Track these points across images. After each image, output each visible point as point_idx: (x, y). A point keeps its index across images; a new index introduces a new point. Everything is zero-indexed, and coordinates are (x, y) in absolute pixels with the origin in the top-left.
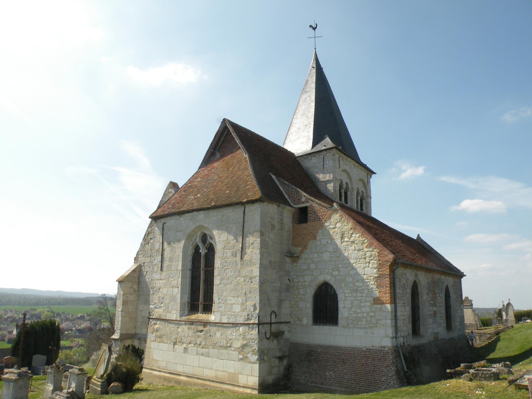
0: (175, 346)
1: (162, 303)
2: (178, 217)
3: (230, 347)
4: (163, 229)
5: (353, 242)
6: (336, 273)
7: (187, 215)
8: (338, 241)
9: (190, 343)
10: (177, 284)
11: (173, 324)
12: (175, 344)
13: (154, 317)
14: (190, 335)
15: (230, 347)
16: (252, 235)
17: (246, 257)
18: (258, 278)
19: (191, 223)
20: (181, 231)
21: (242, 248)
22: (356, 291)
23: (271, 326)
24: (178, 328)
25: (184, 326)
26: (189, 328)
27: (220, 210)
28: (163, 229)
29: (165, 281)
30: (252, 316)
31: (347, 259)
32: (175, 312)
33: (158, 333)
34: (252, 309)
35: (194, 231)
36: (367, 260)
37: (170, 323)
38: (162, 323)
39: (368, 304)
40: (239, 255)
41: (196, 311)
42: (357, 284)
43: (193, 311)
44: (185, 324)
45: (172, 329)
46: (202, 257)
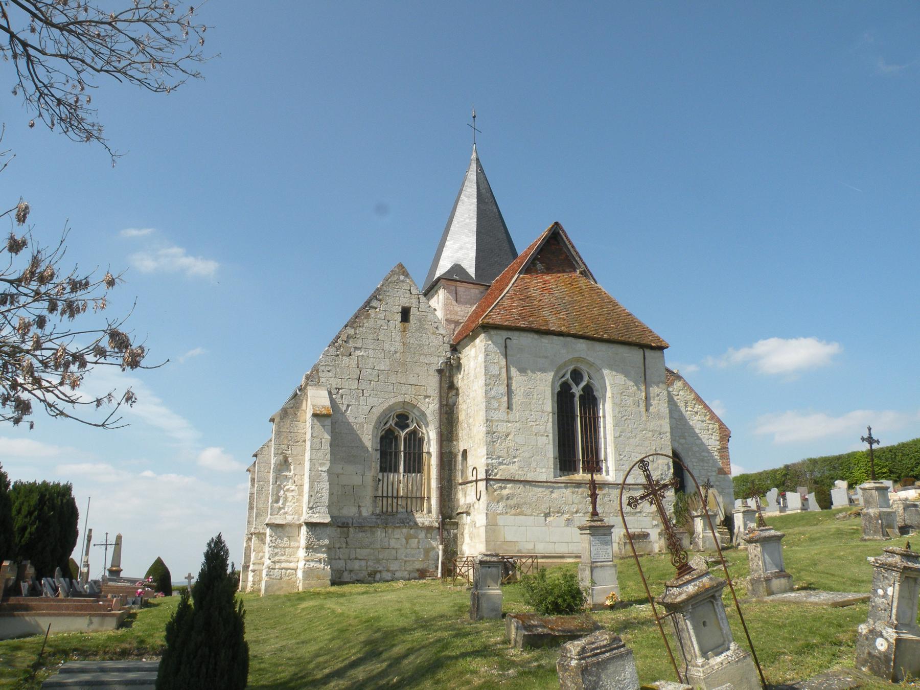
0: (548, 519)
1: (515, 457)
2: (536, 336)
3: (640, 512)
4: (506, 347)
5: (697, 413)
6: (683, 441)
7: (555, 338)
8: (683, 409)
9: (576, 512)
10: (545, 431)
11: (543, 487)
12: (547, 515)
13: (497, 477)
14: (576, 501)
15: (640, 512)
16: (658, 386)
17: (652, 409)
18: (668, 434)
19: (563, 351)
20: (546, 357)
21: (646, 398)
22: (703, 461)
23: (594, 496)
24: (552, 492)
25: (564, 490)
26: (573, 493)
27: (611, 346)
28: (506, 347)
29: (518, 424)
30: (666, 475)
31: (691, 429)
32: (544, 470)
33: (510, 502)
34: (666, 468)
35: (565, 364)
36: (710, 432)
37: (535, 486)
38: (518, 486)
39: (714, 474)
40: (642, 405)
41: (570, 470)
42: (704, 454)
43: (565, 470)
44: (566, 487)
45: (539, 495)
46: (577, 400)
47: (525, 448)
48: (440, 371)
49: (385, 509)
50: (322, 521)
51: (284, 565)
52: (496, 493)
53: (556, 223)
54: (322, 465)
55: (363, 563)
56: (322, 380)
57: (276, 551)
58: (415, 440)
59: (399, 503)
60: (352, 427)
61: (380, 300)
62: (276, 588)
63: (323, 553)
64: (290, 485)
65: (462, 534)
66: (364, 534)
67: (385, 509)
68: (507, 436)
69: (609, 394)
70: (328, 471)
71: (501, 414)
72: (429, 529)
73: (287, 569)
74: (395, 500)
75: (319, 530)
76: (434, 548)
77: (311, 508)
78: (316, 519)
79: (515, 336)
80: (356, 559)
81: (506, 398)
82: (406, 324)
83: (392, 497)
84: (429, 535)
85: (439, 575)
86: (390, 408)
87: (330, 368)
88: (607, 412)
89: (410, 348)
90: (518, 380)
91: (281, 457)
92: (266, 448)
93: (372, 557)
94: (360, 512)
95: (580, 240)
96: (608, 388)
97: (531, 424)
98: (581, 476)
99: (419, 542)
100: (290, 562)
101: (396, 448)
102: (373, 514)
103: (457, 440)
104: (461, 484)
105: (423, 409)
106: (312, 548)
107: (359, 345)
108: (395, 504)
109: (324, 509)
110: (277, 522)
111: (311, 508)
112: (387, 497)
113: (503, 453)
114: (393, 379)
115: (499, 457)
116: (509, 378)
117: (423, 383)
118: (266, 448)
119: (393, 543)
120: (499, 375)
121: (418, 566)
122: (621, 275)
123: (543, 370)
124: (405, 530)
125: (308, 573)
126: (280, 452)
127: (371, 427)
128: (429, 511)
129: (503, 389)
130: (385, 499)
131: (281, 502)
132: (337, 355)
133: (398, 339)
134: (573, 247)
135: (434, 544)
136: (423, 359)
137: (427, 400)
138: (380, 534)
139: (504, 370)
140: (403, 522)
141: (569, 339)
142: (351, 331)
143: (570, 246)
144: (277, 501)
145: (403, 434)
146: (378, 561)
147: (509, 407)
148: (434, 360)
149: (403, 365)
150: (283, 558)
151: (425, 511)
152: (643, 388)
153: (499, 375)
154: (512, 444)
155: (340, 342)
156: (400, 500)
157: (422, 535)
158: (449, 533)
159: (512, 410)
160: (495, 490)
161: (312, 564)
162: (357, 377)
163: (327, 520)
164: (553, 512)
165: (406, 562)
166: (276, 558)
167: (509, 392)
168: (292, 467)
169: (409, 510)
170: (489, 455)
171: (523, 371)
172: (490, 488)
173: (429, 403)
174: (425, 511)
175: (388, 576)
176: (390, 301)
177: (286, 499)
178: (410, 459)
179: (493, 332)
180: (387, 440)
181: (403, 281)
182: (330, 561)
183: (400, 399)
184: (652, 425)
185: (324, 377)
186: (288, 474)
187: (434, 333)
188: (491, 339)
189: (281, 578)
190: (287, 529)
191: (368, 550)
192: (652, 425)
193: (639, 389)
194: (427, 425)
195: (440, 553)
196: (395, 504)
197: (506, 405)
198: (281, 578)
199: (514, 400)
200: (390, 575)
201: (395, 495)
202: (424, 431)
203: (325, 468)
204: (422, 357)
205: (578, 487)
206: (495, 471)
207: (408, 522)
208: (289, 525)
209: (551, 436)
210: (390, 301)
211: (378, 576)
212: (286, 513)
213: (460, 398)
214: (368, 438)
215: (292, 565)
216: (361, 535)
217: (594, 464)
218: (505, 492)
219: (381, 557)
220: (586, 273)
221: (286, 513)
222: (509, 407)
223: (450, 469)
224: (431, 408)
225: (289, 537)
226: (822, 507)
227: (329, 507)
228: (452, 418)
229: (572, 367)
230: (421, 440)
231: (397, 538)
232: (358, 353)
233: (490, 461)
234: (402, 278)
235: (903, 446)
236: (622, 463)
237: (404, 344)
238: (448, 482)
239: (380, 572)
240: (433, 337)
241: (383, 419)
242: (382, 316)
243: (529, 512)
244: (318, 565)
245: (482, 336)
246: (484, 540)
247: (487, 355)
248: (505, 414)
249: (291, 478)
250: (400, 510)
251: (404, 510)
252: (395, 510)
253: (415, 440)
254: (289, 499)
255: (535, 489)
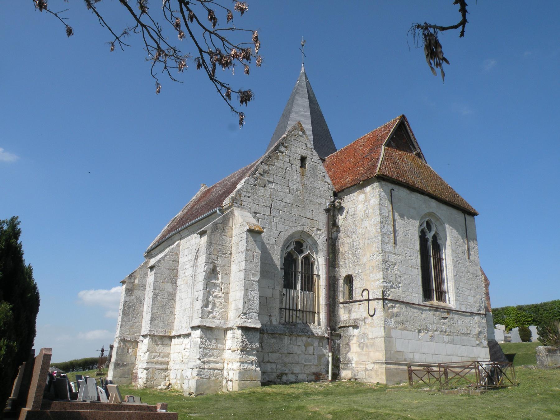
1: (400, 283)
4: (391, 196)
11: (416, 308)
12: (420, 331)
24: (422, 313)
25: (428, 312)
26: (434, 315)
28: (391, 196)
29: (400, 257)
33: (399, 319)
37: (412, 307)
40: (466, 254)
44: (430, 310)
45: (415, 315)
47: (405, 276)
48: (327, 211)
49: (287, 320)
50: (255, 326)
51: (212, 365)
52: (390, 311)
53: (403, 116)
54: (254, 275)
55: (274, 366)
56: (244, 203)
57: (206, 352)
58: (309, 265)
59: (298, 315)
60: (266, 246)
61: (286, 147)
62: (205, 387)
63: (254, 355)
64: (217, 292)
65: (348, 344)
66: (274, 340)
67: (287, 320)
68: (394, 265)
69: (448, 242)
70: (259, 282)
71: (389, 247)
72: (322, 338)
73: (214, 369)
74: (295, 313)
75: (251, 335)
76: (324, 355)
77: (245, 314)
78: (250, 324)
79: (396, 187)
80: (269, 362)
81: (392, 236)
82: (304, 170)
83: (293, 310)
84: (321, 344)
85: (330, 378)
86: (292, 236)
87: (249, 195)
88: (447, 255)
89: (307, 189)
90: (399, 222)
91: (211, 266)
92: (162, 262)
93: (281, 361)
94: (271, 321)
95: (417, 129)
96: (448, 238)
97: (408, 258)
98: (435, 302)
99: (314, 349)
100: (217, 363)
101: (295, 269)
102: (280, 323)
103: (338, 267)
104: (342, 303)
105: (316, 239)
106: (246, 350)
107: (271, 180)
108: (294, 316)
109: (255, 316)
110: (208, 325)
111: (245, 314)
112: (289, 309)
113: (392, 279)
114: (295, 211)
115: (390, 282)
116: (394, 220)
117: (316, 219)
118: (162, 262)
119: (296, 349)
120: (388, 216)
121: (314, 370)
122: (443, 160)
123: (414, 218)
124: (304, 339)
125: (243, 374)
126: (210, 261)
127: (280, 249)
128: (319, 324)
129: (391, 228)
130: (287, 311)
131: (210, 307)
132: (255, 185)
133: (299, 180)
134: (413, 135)
135: (325, 351)
136: (316, 200)
137: (318, 232)
138: (286, 339)
139: (391, 213)
140: (303, 332)
141: (427, 198)
142: (266, 168)
143: (410, 134)
144: (206, 306)
145: (300, 258)
146: (285, 364)
147: (395, 243)
148: (323, 201)
149: (302, 201)
150: (211, 359)
151: (316, 323)
152: (466, 241)
153: (388, 216)
154: (398, 272)
155: (257, 174)
156: (298, 312)
157: (316, 343)
158: (334, 342)
159: (396, 245)
160: (389, 309)
161: (246, 366)
162: (269, 205)
163: (259, 326)
164: (423, 329)
165: (305, 365)
166: (206, 359)
167: (395, 231)
168: (220, 276)
169: (304, 322)
170: (385, 280)
171: (402, 216)
172: (385, 306)
173: (320, 235)
174: (316, 323)
175: (292, 378)
176: (293, 149)
177: (214, 304)
178: (305, 277)
179: (383, 183)
180: (289, 261)
181: (301, 136)
182: (260, 363)
183: (300, 228)
184: (472, 269)
185: (245, 201)
186: (216, 282)
187: (322, 181)
188: (382, 187)
189: (210, 378)
190: (216, 332)
191: (278, 354)
192: (472, 269)
193: (464, 242)
194: (317, 253)
195: (330, 359)
196: (294, 316)
197: (393, 241)
198: (210, 378)
199: (397, 238)
200: (294, 377)
201: (295, 308)
202: (315, 257)
203: (256, 279)
204: (315, 197)
205: (437, 311)
206: (388, 292)
207: (307, 332)
208: (217, 328)
209: (420, 268)
210: (293, 149)
211: (284, 378)
212: (214, 317)
213: (341, 234)
214: (277, 260)
215: (219, 366)
216: (273, 341)
217: (441, 296)
218: (395, 310)
219: (287, 361)
220: (419, 155)
221: (214, 317)
222: (395, 243)
223: (334, 291)
224: (321, 238)
225: (216, 339)
226: (523, 340)
227: (259, 314)
228: (335, 249)
229: (427, 219)
230: (312, 264)
231: (297, 346)
232: (270, 186)
233: (385, 284)
234: (301, 133)
235: (545, 304)
236: (458, 295)
237: (303, 185)
238: (333, 301)
239: (286, 374)
240: (322, 183)
241: (286, 245)
242: (287, 159)
243: (409, 328)
244: (250, 366)
245: (376, 184)
246: (384, 349)
247: (381, 200)
248: (393, 247)
249: (219, 286)
250: (298, 321)
251: (301, 322)
252: (294, 321)
253: (309, 265)
254: (217, 305)
255: (412, 309)
